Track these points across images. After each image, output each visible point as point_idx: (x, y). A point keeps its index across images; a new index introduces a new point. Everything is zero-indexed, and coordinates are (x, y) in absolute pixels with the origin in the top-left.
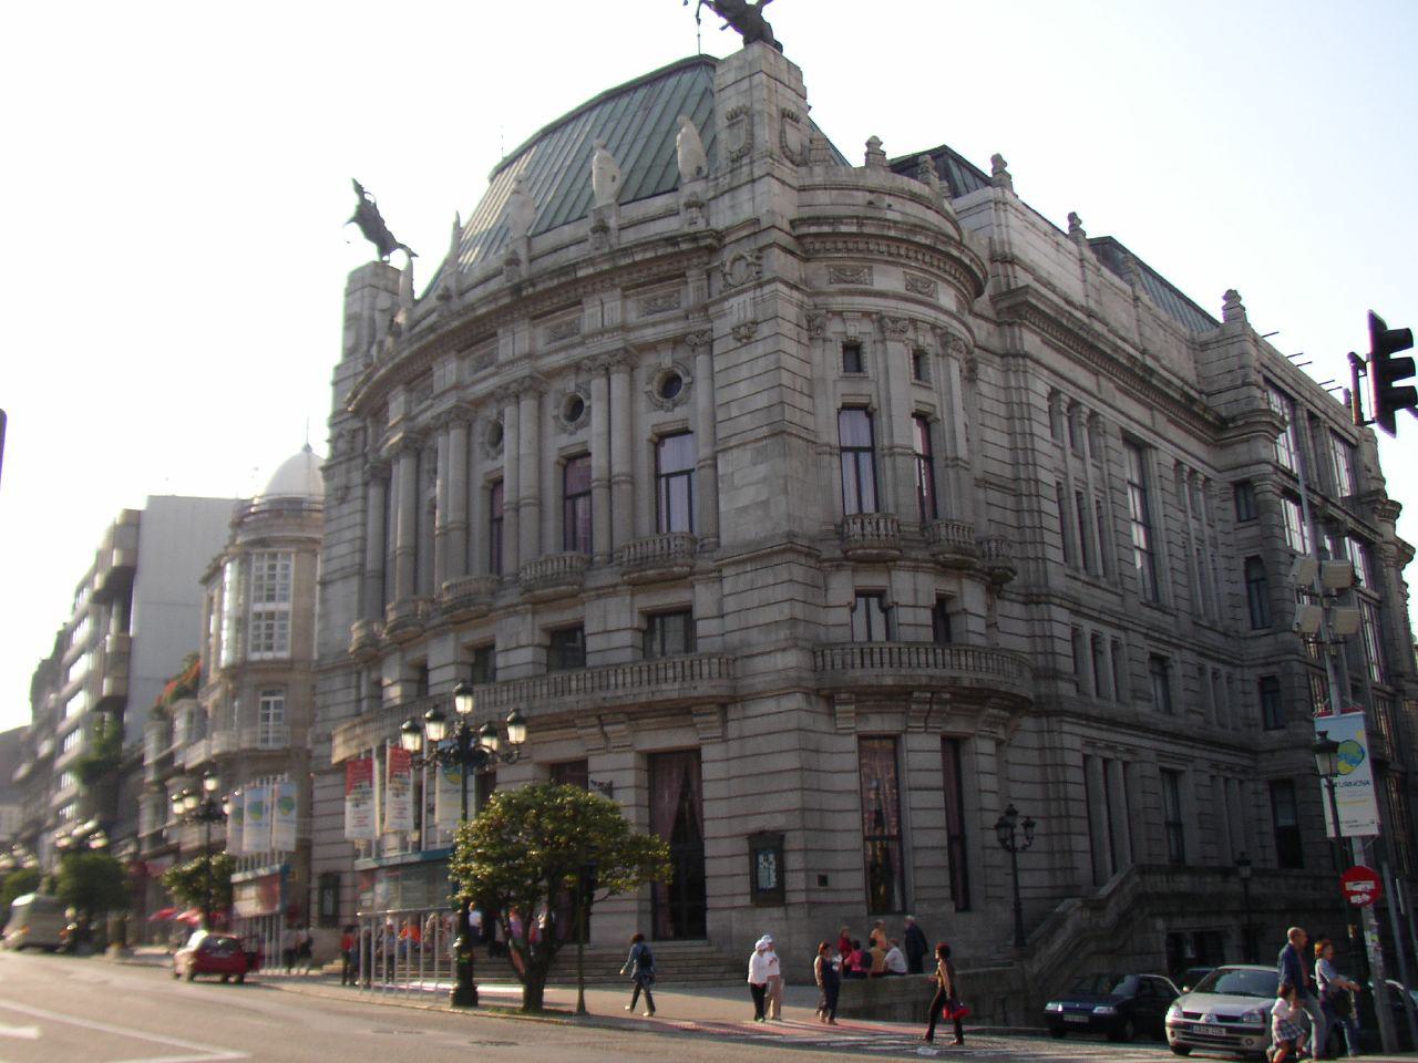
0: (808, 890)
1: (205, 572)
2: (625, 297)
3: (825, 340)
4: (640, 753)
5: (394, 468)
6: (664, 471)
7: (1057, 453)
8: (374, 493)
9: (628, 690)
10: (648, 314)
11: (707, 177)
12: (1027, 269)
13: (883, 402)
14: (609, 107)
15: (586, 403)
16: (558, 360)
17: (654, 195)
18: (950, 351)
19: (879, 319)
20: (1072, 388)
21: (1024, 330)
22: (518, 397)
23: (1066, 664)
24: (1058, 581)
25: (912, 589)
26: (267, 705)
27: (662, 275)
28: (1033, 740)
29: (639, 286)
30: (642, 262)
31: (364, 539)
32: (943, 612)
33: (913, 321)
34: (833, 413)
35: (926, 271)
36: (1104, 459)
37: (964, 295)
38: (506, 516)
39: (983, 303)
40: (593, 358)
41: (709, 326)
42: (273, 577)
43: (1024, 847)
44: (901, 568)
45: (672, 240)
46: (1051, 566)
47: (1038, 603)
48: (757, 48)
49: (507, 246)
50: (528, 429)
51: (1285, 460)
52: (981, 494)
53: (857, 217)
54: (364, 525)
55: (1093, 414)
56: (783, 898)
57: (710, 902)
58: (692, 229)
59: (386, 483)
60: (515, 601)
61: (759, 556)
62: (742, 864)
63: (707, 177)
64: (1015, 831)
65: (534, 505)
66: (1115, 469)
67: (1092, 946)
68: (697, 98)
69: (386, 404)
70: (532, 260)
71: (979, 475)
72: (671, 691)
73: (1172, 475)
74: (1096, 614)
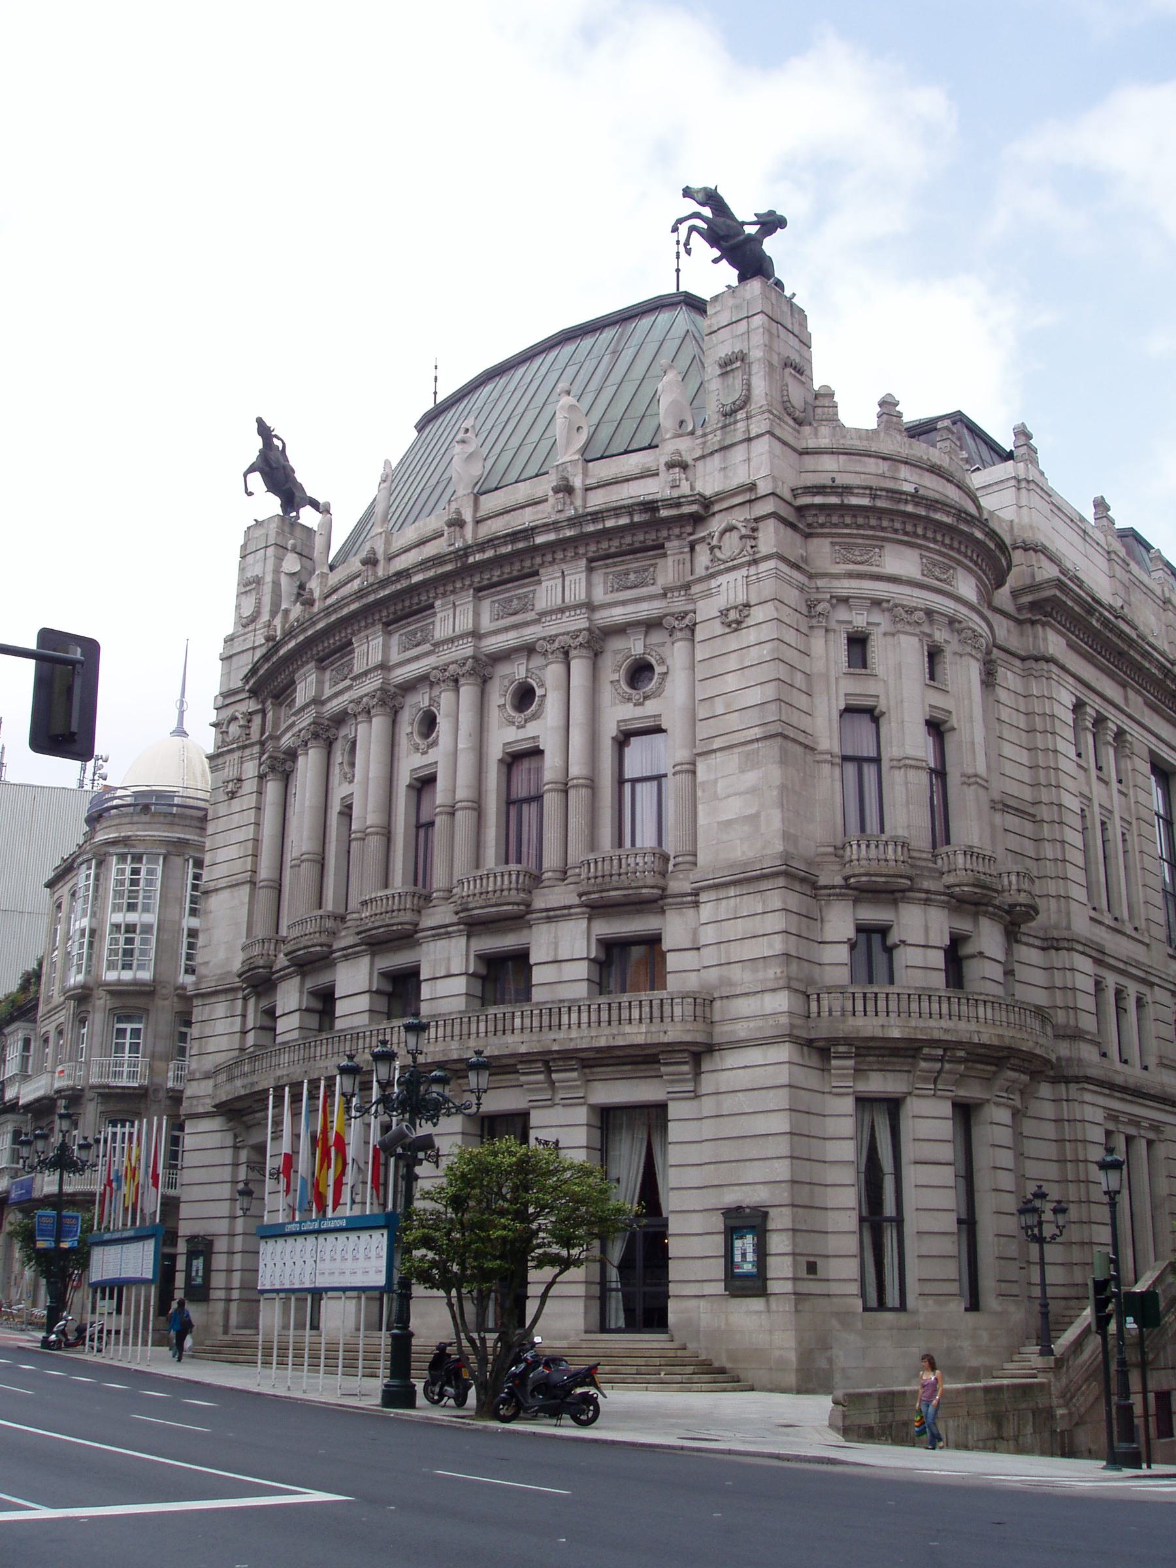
0: (795, 1279)
2: (590, 570)
4: (592, 1107)
5: (301, 759)
6: (628, 775)
8: (272, 788)
11: (692, 433)
14: (569, 348)
17: (626, 452)
20: (1098, 700)
21: (1048, 629)
22: (456, 681)
23: (1088, 1023)
25: (920, 929)
26: (121, 1033)
27: (637, 545)
29: (608, 557)
30: (612, 528)
31: (256, 841)
32: (955, 957)
33: (929, 613)
34: (835, 715)
36: (1131, 784)
37: (985, 586)
38: (438, 820)
39: (1003, 596)
40: (551, 639)
41: (690, 607)
42: (134, 883)
43: (1053, 1237)
44: (911, 901)
45: (650, 506)
46: (1074, 906)
47: (1057, 949)
48: (755, 286)
52: (998, 818)
53: (871, 488)
54: (257, 824)
56: (765, 1288)
57: (673, 1289)
58: (676, 493)
59: (286, 778)
60: (447, 922)
61: (747, 880)
64: (1044, 1217)
65: (473, 809)
68: (677, 342)
69: (292, 683)
70: (478, 522)
71: (997, 797)
72: (636, 1034)
74: (1122, 966)
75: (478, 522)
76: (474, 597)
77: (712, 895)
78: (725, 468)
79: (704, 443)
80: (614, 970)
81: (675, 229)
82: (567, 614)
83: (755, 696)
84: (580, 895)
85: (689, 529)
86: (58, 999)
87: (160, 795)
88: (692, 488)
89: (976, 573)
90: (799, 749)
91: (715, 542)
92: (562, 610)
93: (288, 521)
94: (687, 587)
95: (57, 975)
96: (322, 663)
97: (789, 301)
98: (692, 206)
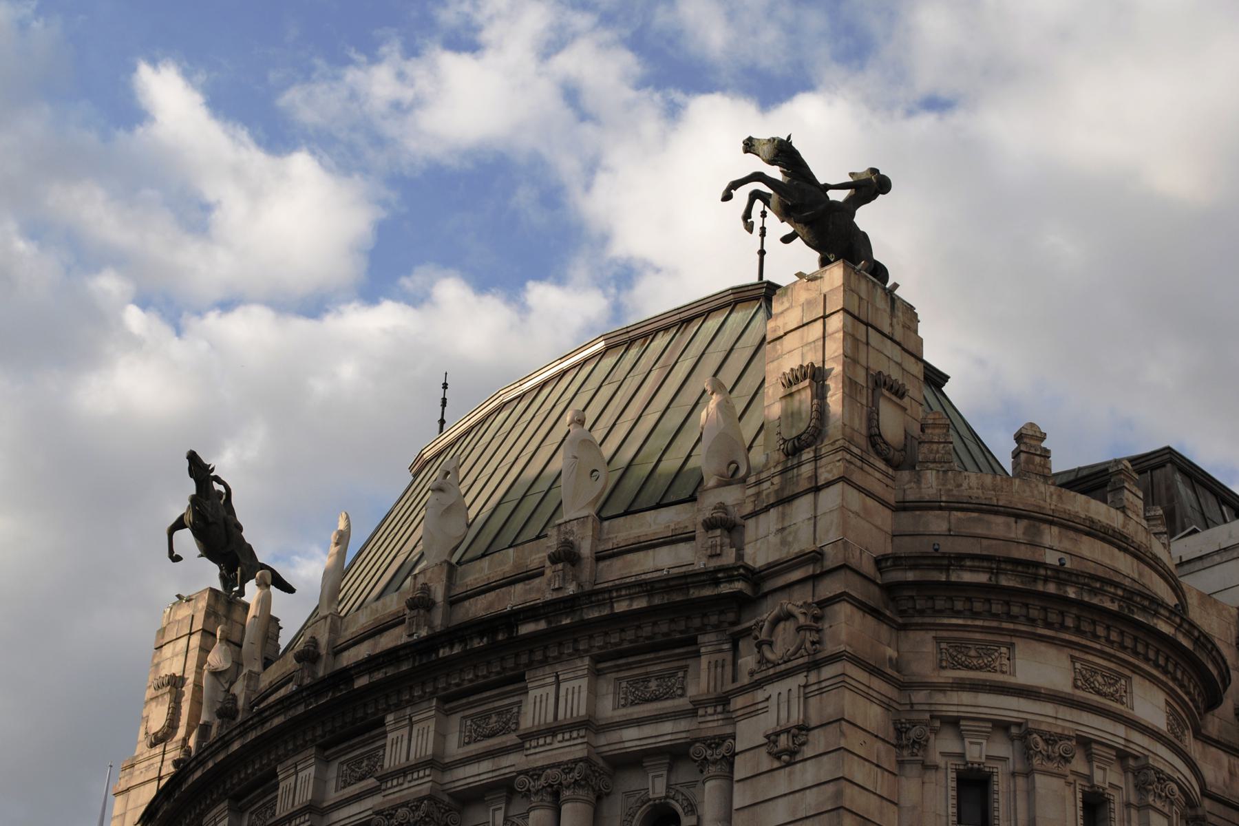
3: (927, 767)
10: (633, 704)
11: (743, 480)
16: (480, 772)
17: (659, 506)
18: (1151, 799)
19: (1016, 732)
22: (556, 795)
27: (659, 639)
33: (1085, 743)
41: (728, 730)
49: (415, 577)
58: (714, 563)
63: (743, 480)
70: (453, 602)
76: (438, 709)
78: (783, 529)
79: (758, 494)
81: (727, 197)
82: (560, 737)
85: (731, 616)
88: (740, 556)
89: (1165, 684)
91: (763, 636)
93: (225, 604)
94: (723, 700)
97: (890, 294)
98: (755, 164)
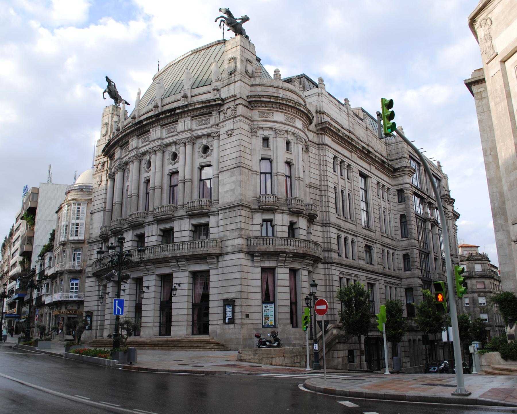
1: (57, 209)
3: (256, 137)
4: (190, 272)
7: (335, 177)
9: (184, 251)
12: (328, 116)
13: (275, 158)
15: (178, 155)
22: (156, 152)
23: (335, 247)
24: (333, 219)
25: (282, 220)
28: (322, 271)
31: (106, 198)
32: (292, 228)
33: (287, 131)
35: (292, 115)
39: (312, 127)
40: (181, 140)
46: (331, 214)
47: (326, 226)
50: (159, 163)
51: (415, 183)
52: (308, 190)
54: (106, 194)
55: (349, 165)
58: (215, 98)
59: (114, 180)
62: (221, 310)
66: (355, 183)
67: (337, 341)
69: (114, 153)
71: (308, 184)
72: (201, 251)
73: (376, 186)
74: (346, 231)
75: (163, 106)
77: (222, 212)
80: (198, 233)
81: (216, 21)
83: (234, 156)
84: (187, 212)
85: (218, 108)
86: (58, 245)
87: (86, 186)
88: (220, 96)
90: (247, 170)
91: (225, 112)
92: (184, 132)
93: (116, 107)
94: (217, 125)
95: (58, 239)
96: (122, 147)
98: (222, 14)
